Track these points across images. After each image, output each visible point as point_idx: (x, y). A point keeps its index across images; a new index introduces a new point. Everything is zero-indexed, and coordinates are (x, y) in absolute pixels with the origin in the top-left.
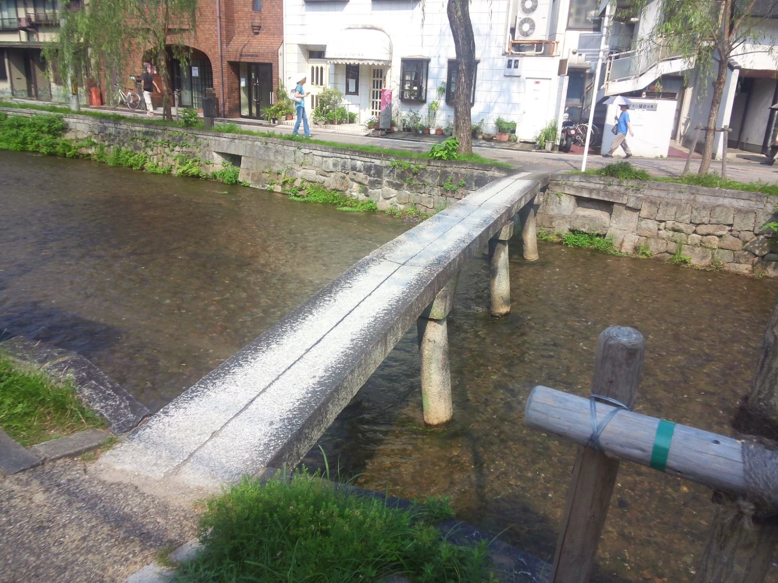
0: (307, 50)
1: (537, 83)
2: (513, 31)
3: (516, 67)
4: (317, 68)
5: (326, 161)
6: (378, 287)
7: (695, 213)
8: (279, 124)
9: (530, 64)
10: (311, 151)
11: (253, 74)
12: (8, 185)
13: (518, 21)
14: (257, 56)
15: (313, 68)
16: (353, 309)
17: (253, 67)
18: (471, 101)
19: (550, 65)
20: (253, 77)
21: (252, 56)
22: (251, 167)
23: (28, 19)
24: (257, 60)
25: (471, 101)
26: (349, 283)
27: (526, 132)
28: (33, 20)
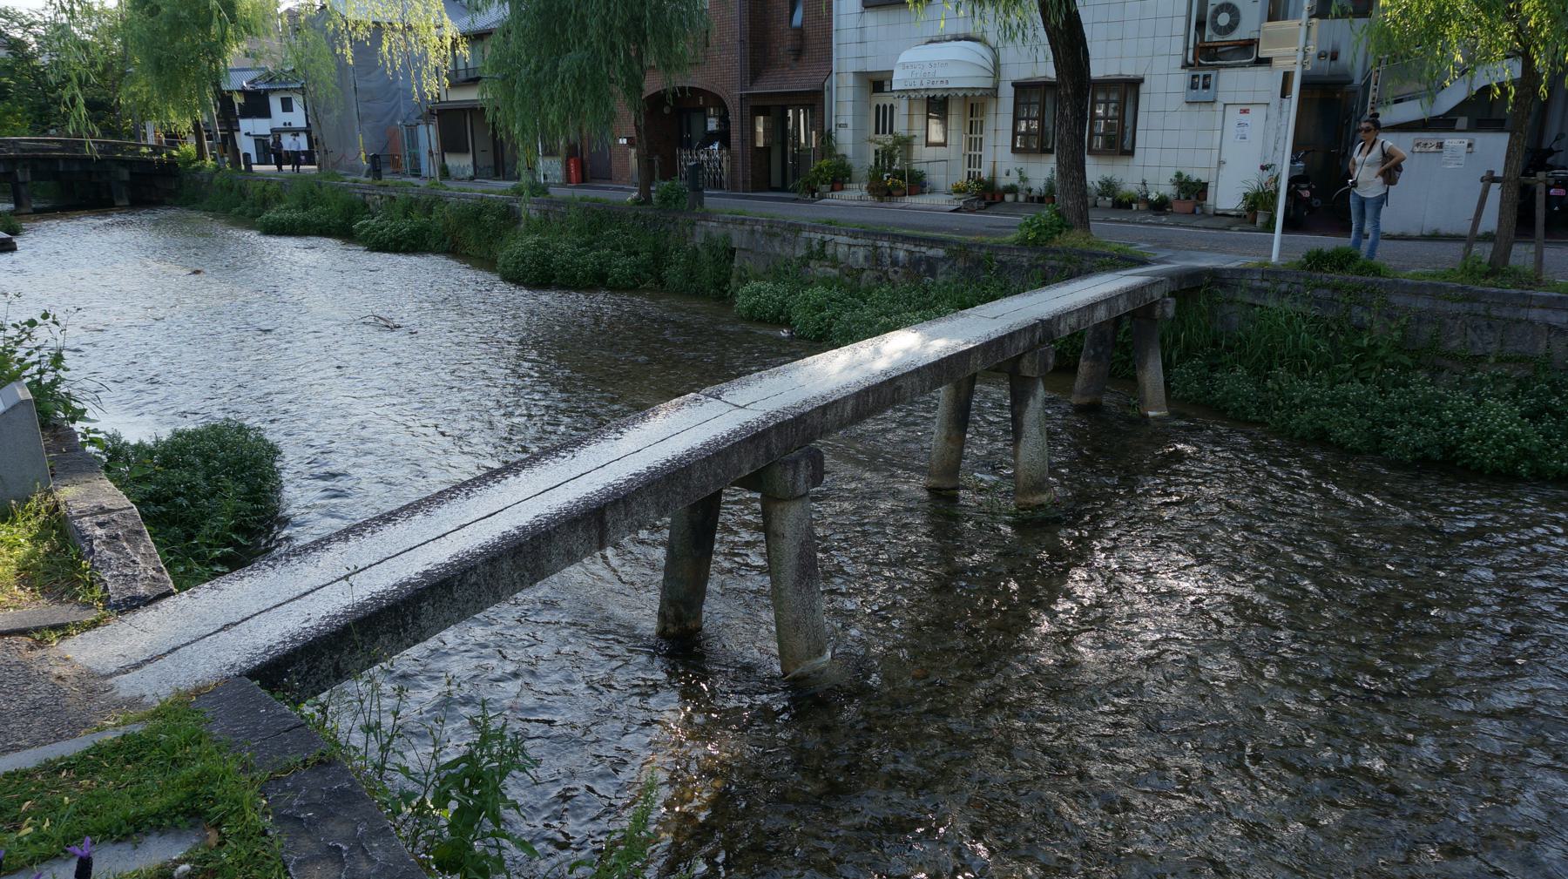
1: (1245, 111)
2: (1201, 25)
3: (1206, 87)
4: (885, 106)
7: (1472, 335)
9: (1234, 81)
12: (21, 271)
13: (1210, 10)
15: (878, 107)
18: (656, 158)
19: (1264, 82)
25: (656, 158)
27: (1227, 196)
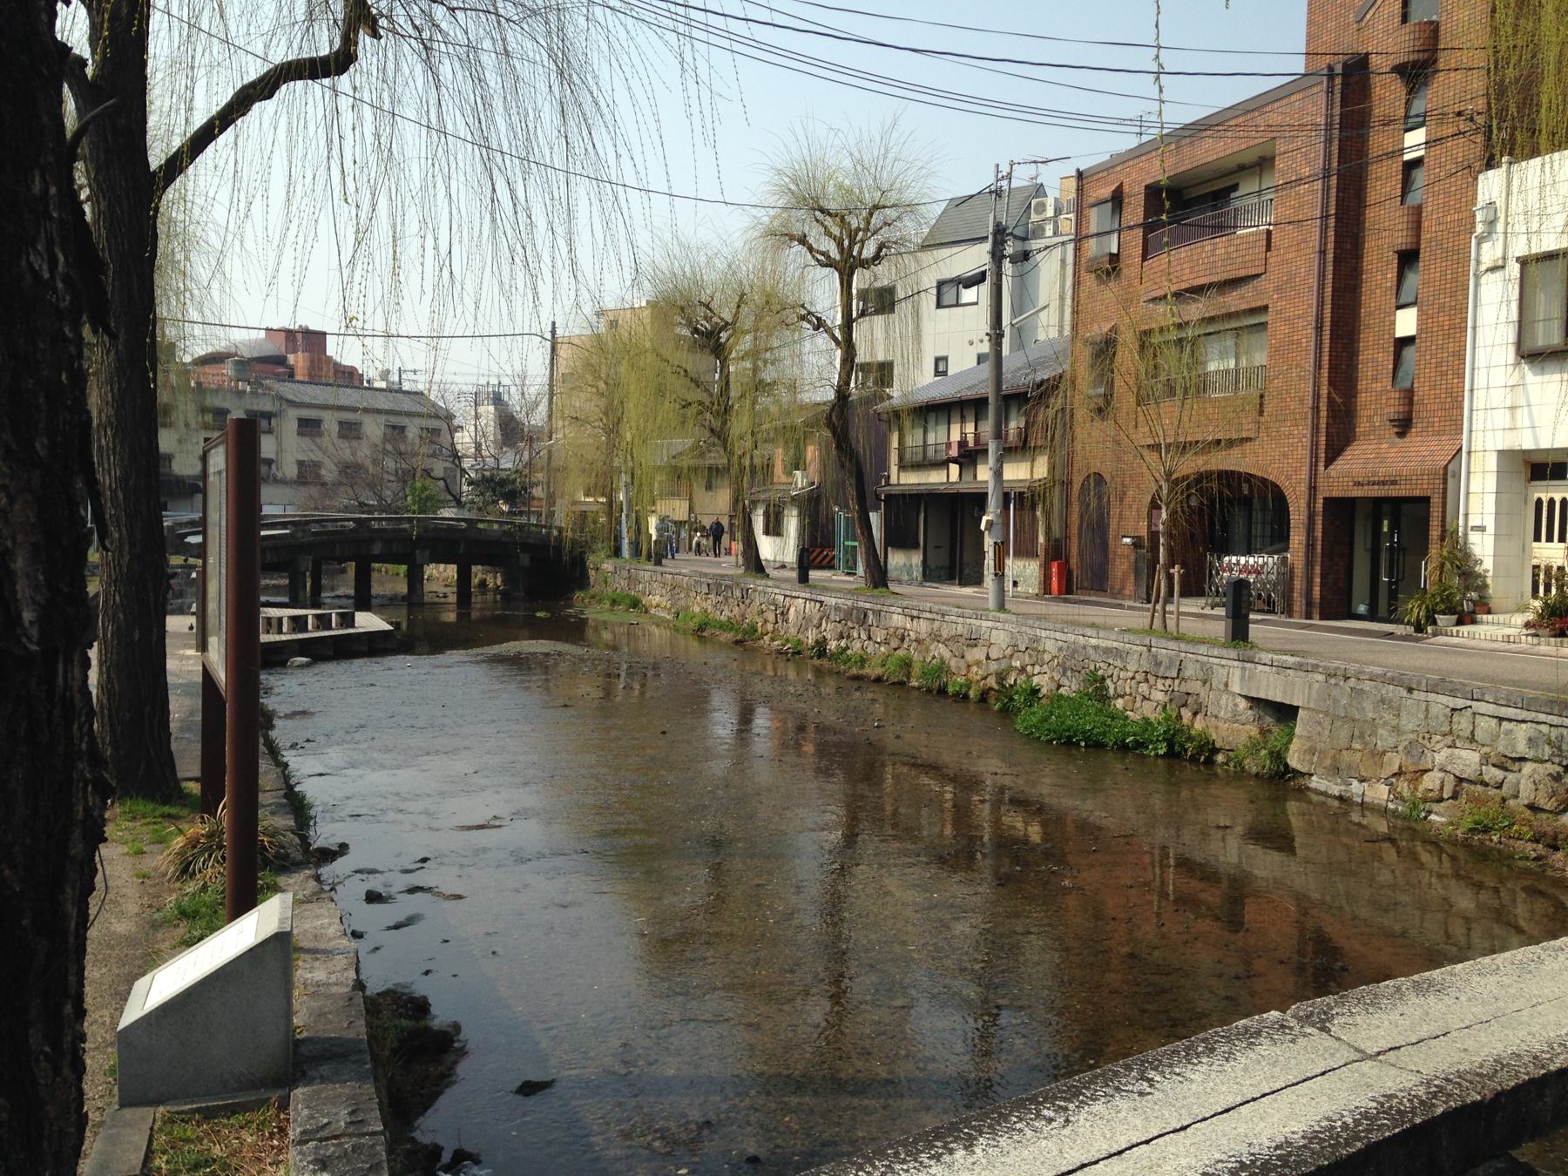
0: (1526, 462)
5: (1509, 732)
6: (1227, 1111)
8: (1435, 635)
10: (1469, 703)
11: (1386, 522)
14: (1394, 483)
16: (1096, 1162)
17: (1386, 508)
20: (1385, 529)
21: (1384, 483)
22: (1319, 733)
23: (962, 444)
24: (1394, 492)
26: (1150, 1080)
28: (971, 444)
